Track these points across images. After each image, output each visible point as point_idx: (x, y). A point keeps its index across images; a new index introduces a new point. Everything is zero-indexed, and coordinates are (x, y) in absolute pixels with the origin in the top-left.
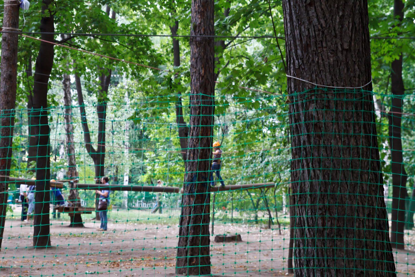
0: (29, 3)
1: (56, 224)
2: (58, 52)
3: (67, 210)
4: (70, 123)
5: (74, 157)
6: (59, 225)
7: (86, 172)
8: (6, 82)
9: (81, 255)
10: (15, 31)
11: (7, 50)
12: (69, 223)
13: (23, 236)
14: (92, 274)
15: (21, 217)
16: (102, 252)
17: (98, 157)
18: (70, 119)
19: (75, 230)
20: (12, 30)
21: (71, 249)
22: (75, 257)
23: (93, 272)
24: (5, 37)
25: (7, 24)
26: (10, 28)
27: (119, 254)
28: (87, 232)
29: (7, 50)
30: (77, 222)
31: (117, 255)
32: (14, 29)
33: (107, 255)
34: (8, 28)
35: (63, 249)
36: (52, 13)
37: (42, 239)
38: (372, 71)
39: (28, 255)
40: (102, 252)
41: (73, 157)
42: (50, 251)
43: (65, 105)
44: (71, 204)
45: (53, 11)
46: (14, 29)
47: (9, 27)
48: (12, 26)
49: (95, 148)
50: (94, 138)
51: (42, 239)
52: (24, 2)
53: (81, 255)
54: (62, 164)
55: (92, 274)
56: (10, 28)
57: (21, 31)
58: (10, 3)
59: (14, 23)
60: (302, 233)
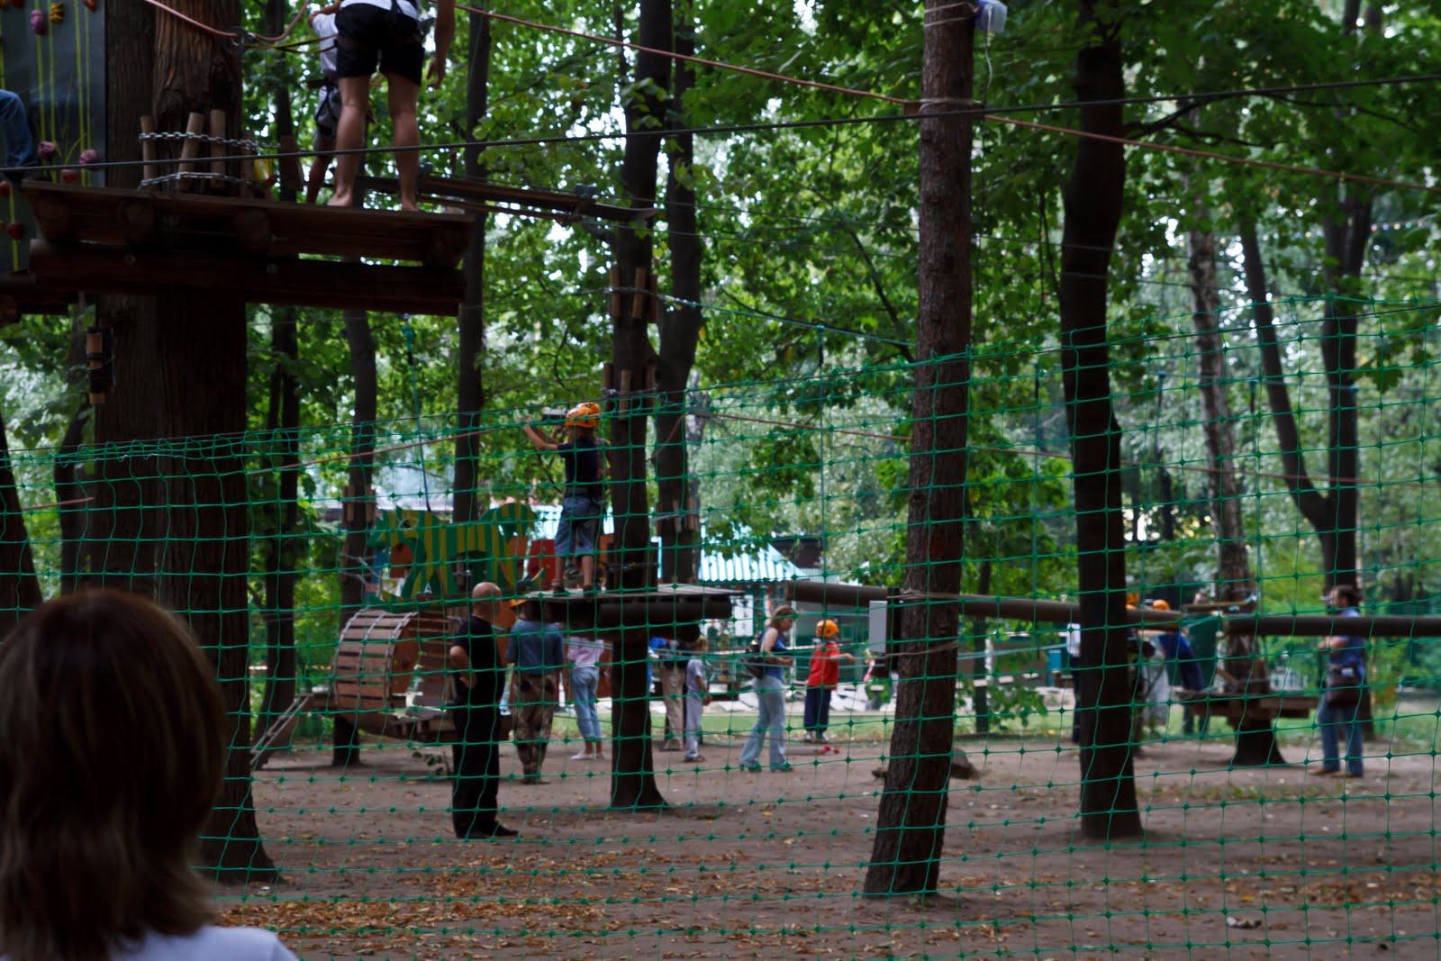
0: (1004, 8)
1: (1190, 752)
2: (1154, 162)
3: (1220, 706)
4: (1218, 403)
5: (1239, 523)
6: (1180, 758)
7: (1287, 567)
8: (936, 280)
9: (1241, 860)
10: (960, 107)
11: (936, 174)
12: (1230, 750)
13: (1065, 795)
14: (1247, 926)
15: (1070, 732)
16: (1319, 852)
17: (1332, 515)
18: (1217, 390)
19: (1247, 777)
20: (950, 106)
21: (1213, 839)
22: (1216, 870)
23: (1252, 922)
24: (930, 133)
25: (936, 86)
26: (945, 99)
27: (1379, 861)
28: (1291, 783)
29: (936, 174)
30: (1258, 747)
31: (1370, 864)
32: (959, 101)
33: (1332, 862)
34: (937, 101)
35: (1183, 840)
36: (1110, 33)
37: (1109, 807)
38: (1262, 251)
39: (1057, 858)
40: (1319, 852)
41: (1234, 522)
42: (1134, 847)
43: (1199, 343)
44: (1235, 682)
45: (1110, 26)
46: (959, 101)
47: (940, 95)
48: (949, 95)
49: (1322, 486)
50: (1317, 455)
51: (1109, 807)
52: (988, 9)
53: (1241, 860)
54: (1198, 547)
55: (1247, 926)
56: (945, 99)
57: (982, 106)
58: (944, 17)
59: (958, 77)
60: (797, 810)
